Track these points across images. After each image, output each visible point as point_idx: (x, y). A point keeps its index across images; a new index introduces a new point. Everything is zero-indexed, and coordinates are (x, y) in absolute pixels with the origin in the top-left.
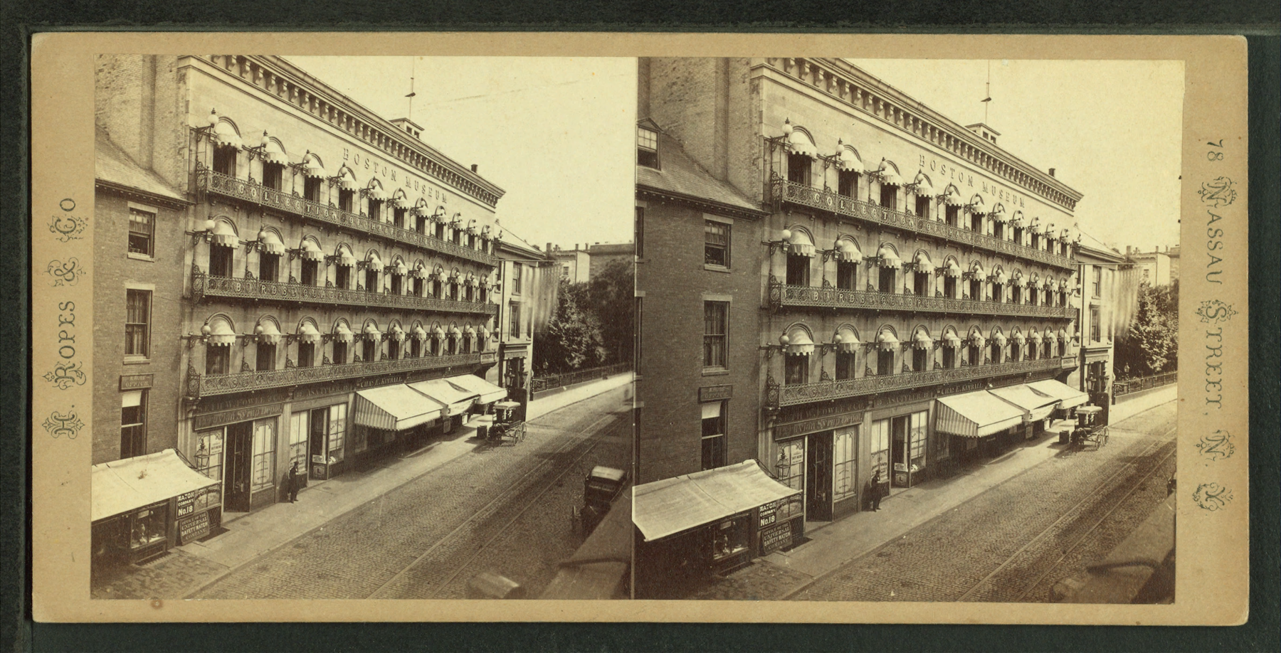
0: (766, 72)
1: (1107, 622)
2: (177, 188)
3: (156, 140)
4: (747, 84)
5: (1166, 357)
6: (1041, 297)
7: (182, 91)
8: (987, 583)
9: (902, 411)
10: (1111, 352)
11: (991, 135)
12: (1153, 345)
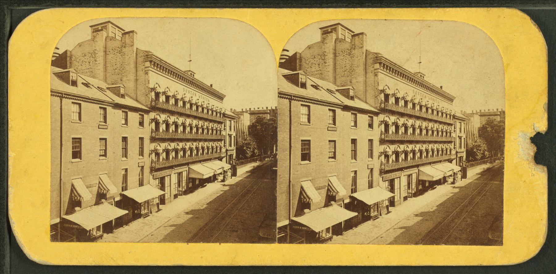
1: (443, 248)
2: (146, 106)
5: (482, 154)
7: (147, 77)
9: (180, 171)
11: (422, 76)
12: (247, 148)
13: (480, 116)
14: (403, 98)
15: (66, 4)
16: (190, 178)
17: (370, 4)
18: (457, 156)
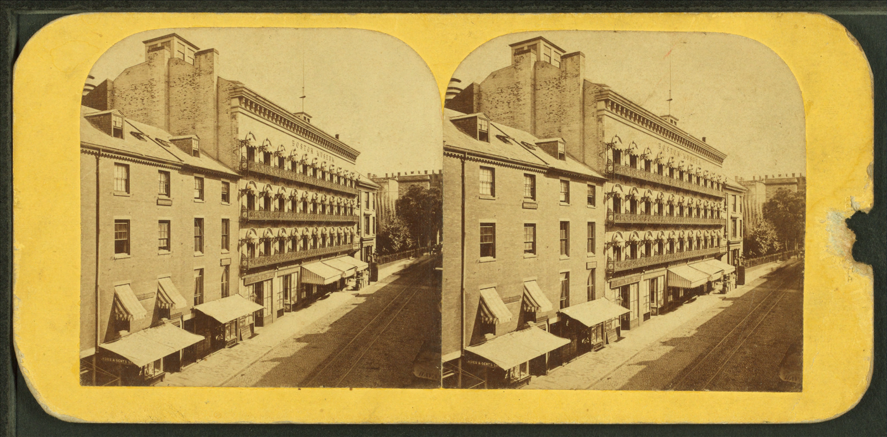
0: (605, 112)
1: (706, 395)
2: (234, 169)
3: (586, 149)
4: (595, 117)
6: (666, 209)
8: (256, 379)
9: (287, 272)
10: (742, 243)
12: (395, 235)
13: (766, 184)
14: (643, 156)
15: (105, 6)
16: (302, 285)
17: (591, 7)
18: (729, 248)
